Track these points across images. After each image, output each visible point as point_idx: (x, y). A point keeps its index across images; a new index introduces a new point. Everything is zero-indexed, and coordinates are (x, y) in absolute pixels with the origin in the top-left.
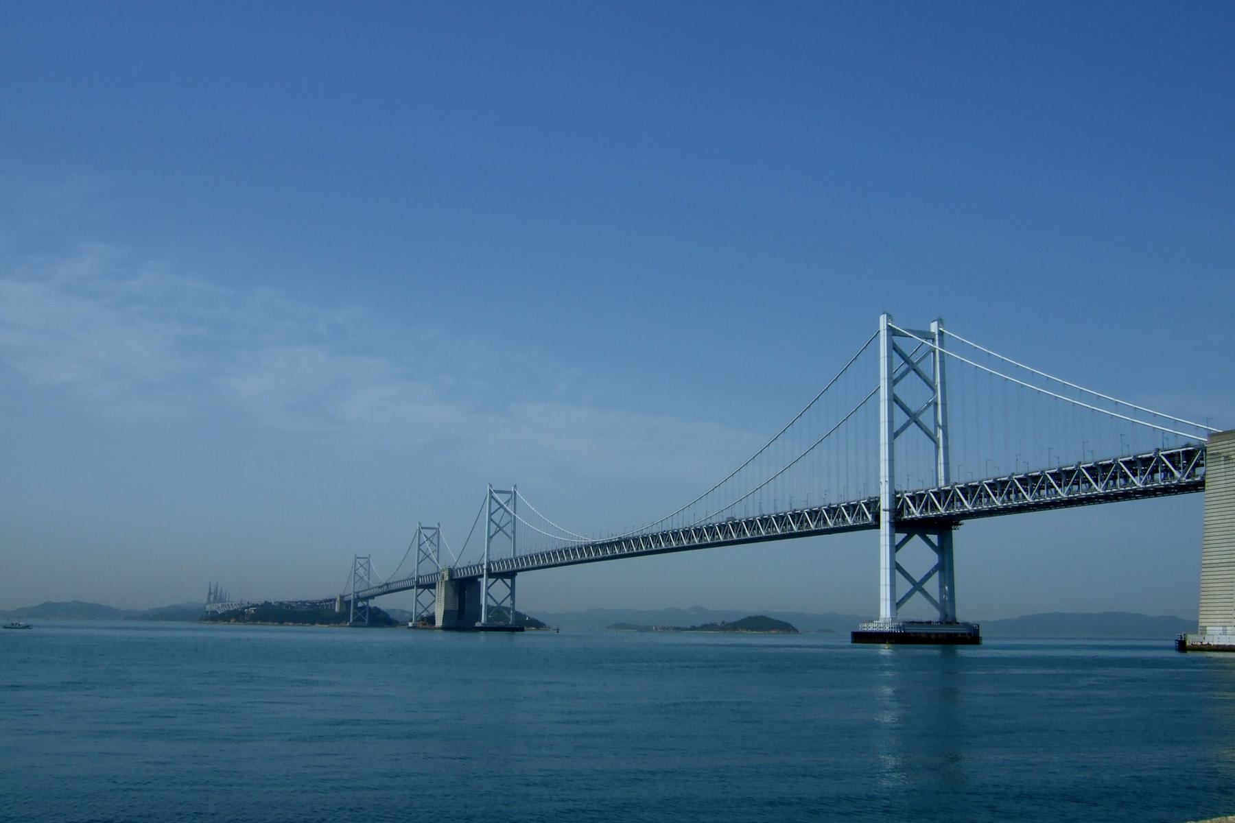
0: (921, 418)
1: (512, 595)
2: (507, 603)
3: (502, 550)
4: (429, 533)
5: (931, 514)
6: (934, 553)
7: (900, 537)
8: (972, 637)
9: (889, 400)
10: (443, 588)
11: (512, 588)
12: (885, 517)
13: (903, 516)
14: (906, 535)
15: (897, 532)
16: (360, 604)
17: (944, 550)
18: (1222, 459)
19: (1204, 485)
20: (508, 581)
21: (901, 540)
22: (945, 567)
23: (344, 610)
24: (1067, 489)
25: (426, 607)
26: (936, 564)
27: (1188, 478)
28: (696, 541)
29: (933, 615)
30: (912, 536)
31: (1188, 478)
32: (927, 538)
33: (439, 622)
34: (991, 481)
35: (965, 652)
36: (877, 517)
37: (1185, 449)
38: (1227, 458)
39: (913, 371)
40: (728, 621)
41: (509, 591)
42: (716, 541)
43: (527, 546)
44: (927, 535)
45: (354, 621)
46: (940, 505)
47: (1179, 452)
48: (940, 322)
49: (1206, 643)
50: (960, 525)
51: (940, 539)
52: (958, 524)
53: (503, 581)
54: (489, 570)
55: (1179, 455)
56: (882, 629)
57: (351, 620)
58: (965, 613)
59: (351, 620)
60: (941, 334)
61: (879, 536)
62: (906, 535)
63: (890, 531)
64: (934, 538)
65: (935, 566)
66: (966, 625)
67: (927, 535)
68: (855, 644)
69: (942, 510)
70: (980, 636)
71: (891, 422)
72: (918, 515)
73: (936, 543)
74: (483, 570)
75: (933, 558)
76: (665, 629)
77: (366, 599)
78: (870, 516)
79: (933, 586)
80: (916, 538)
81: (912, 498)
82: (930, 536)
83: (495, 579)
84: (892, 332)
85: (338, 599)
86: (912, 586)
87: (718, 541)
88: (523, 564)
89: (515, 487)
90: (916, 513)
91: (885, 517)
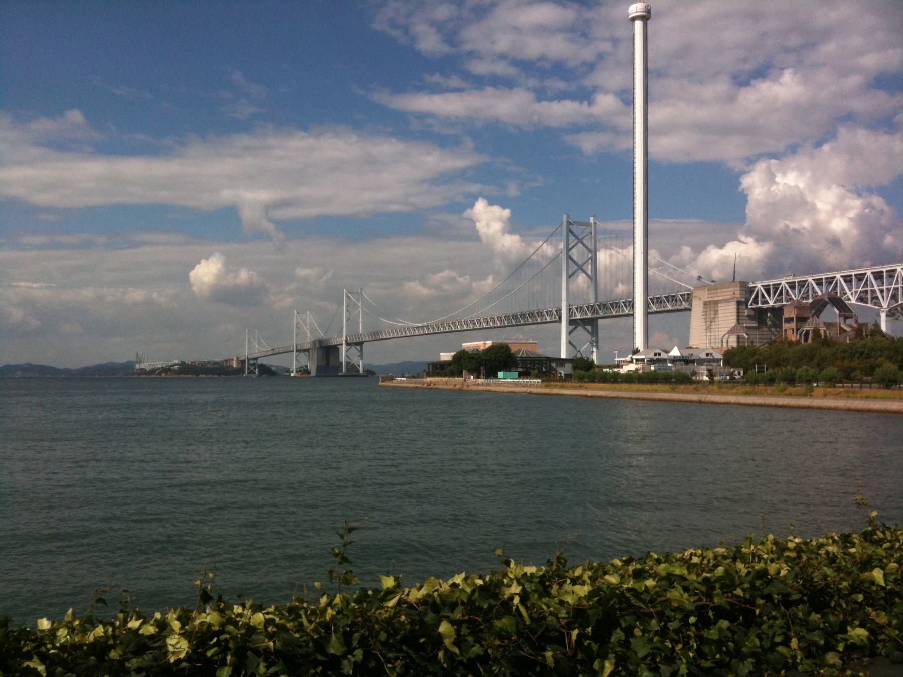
0: (576, 267)
5: (585, 317)
7: (572, 327)
9: (567, 259)
10: (315, 352)
16: (252, 362)
20: (358, 347)
23: (240, 366)
24: (616, 310)
34: (667, 295)
36: (560, 318)
38: (700, 299)
40: (458, 94)
45: (248, 373)
48: (595, 216)
54: (346, 341)
57: (246, 372)
59: (246, 372)
60: (595, 223)
61: (561, 327)
64: (589, 328)
71: (568, 270)
73: (590, 331)
74: (342, 340)
77: (256, 359)
78: (557, 317)
80: (580, 328)
81: (577, 309)
82: (587, 327)
84: (569, 223)
85: (235, 359)
87: (406, 598)
88: (397, 334)
89: (361, 289)
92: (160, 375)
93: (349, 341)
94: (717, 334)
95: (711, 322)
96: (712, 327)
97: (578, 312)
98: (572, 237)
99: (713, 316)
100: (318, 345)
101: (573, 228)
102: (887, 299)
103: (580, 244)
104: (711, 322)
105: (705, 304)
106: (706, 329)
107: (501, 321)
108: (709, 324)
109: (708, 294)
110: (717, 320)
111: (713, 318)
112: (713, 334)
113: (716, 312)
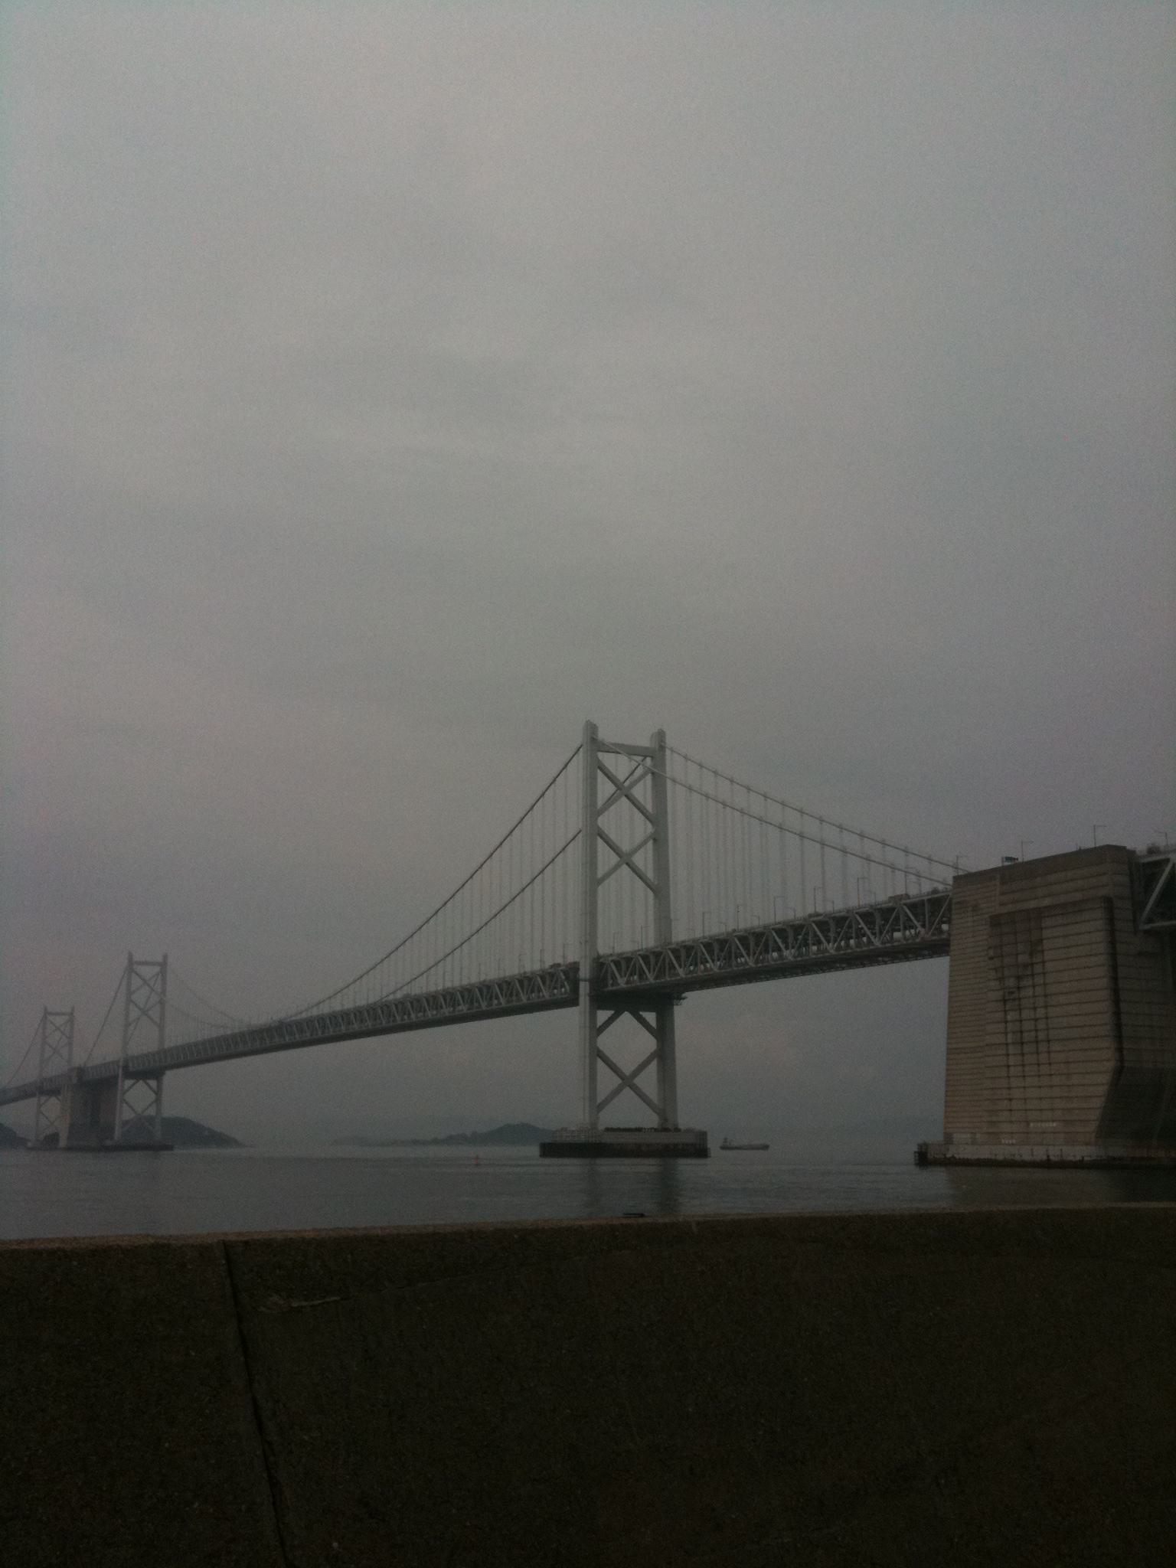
0: (614, 859)
1: (158, 1101)
2: (152, 1112)
3: (145, 1042)
4: (148, 972)
6: (653, 1038)
7: (603, 1015)
8: (698, 1150)
11: (158, 1092)
12: (584, 988)
13: (607, 986)
14: (613, 1012)
15: (600, 1008)
17: (663, 1033)
18: (970, 909)
19: (948, 945)
20: (153, 1083)
21: (607, 1018)
22: (664, 1054)
25: (627, 1070)
26: (652, 1050)
27: (933, 934)
28: (484, 1005)
29: (651, 1120)
30: (621, 1014)
31: (933, 934)
32: (641, 1016)
33: (63, 1142)
35: (686, 1168)
37: (930, 897)
39: (624, 799)
41: (153, 1096)
42: (514, 1003)
43: (178, 1035)
44: (641, 1013)
46: (650, 972)
47: (923, 901)
49: (951, 1156)
50: (684, 999)
51: (658, 1020)
52: (680, 998)
53: (147, 1084)
55: (923, 905)
56: (576, 1139)
58: (688, 1117)
62: (613, 1012)
63: (590, 1008)
64: (651, 1017)
65: (652, 1054)
66: (688, 1131)
67: (641, 1013)
68: (547, 1161)
69: (651, 978)
70: (709, 1146)
72: (753, 965)
75: (647, 1043)
76: (436, 1142)
79: (649, 1081)
82: (126, 1087)
83: (132, 1081)
86: (620, 1081)
90: (622, 983)
91: (584, 988)
92: (798, 939)
93: (131, 1069)
94: (1041, 1013)
95: (1019, 978)
96: (1023, 993)
97: (619, 970)
98: (602, 781)
99: (1023, 958)
100: (75, 1081)
101: (607, 759)
102: (654, 971)
103: (625, 867)
104: (1019, 978)
105: (996, 921)
106: (1005, 1001)
107: (349, 1023)
108: (1011, 983)
109: (1003, 894)
110: (1038, 969)
111: (1025, 966)
112: (1026, 1014)
113: (1035, 947)
